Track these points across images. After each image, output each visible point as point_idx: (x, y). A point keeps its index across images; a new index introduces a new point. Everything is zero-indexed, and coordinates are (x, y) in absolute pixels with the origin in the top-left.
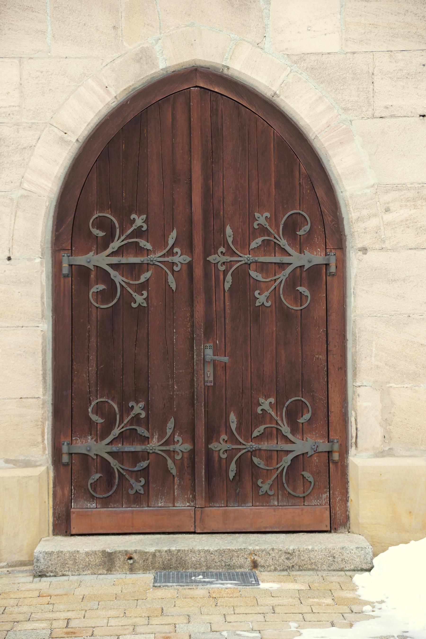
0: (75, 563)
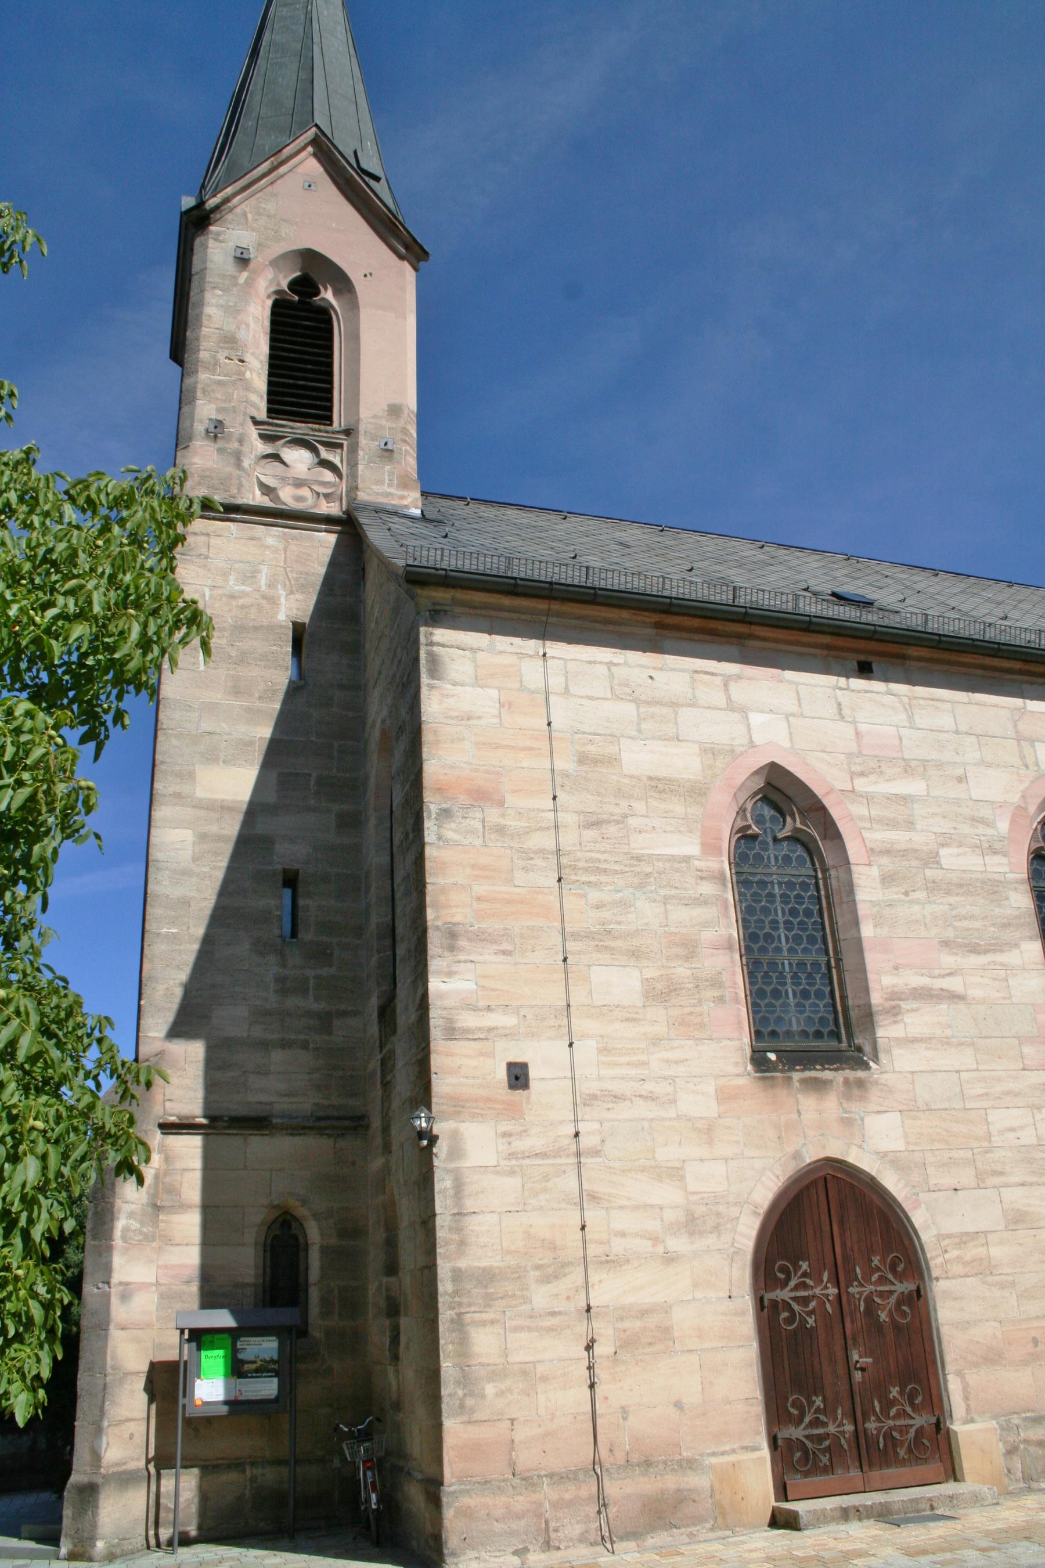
0: (825, 1517)
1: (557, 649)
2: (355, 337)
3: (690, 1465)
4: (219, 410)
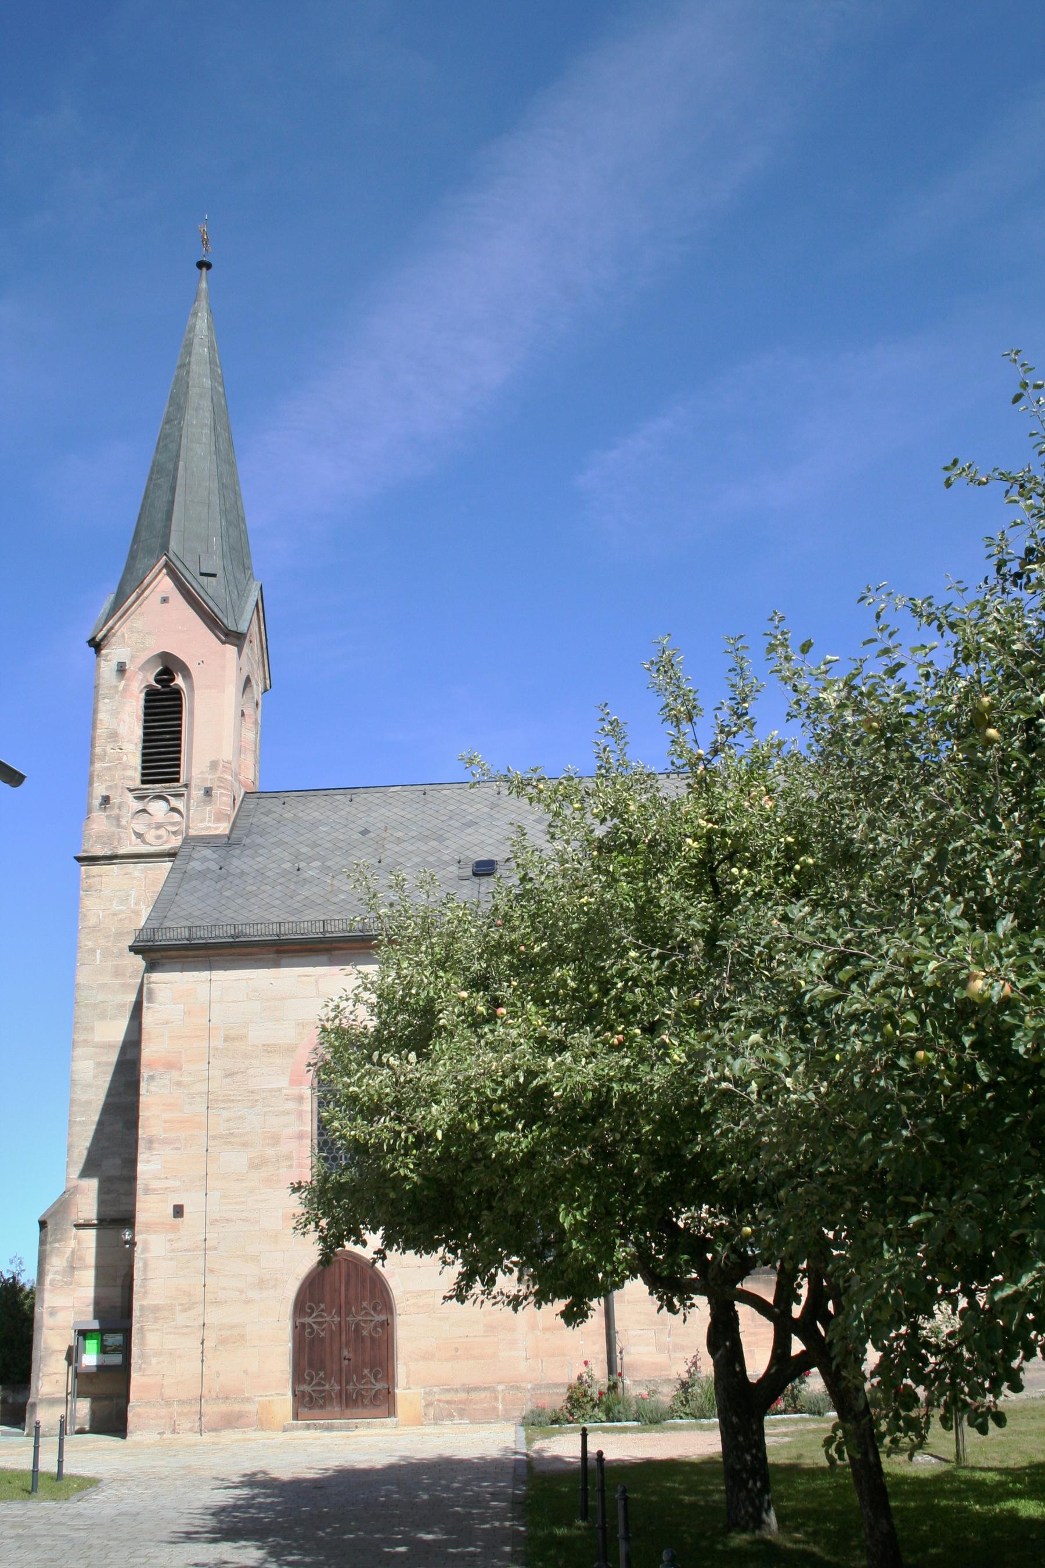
1: (219, 975)
2: (191, 713)
3: (248, 1400)
4: (108, 788)
